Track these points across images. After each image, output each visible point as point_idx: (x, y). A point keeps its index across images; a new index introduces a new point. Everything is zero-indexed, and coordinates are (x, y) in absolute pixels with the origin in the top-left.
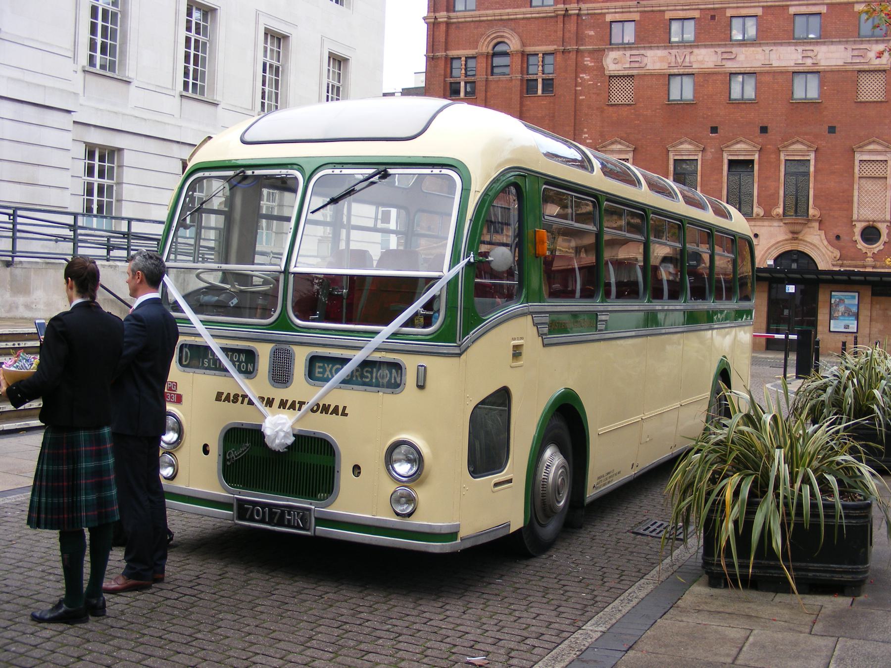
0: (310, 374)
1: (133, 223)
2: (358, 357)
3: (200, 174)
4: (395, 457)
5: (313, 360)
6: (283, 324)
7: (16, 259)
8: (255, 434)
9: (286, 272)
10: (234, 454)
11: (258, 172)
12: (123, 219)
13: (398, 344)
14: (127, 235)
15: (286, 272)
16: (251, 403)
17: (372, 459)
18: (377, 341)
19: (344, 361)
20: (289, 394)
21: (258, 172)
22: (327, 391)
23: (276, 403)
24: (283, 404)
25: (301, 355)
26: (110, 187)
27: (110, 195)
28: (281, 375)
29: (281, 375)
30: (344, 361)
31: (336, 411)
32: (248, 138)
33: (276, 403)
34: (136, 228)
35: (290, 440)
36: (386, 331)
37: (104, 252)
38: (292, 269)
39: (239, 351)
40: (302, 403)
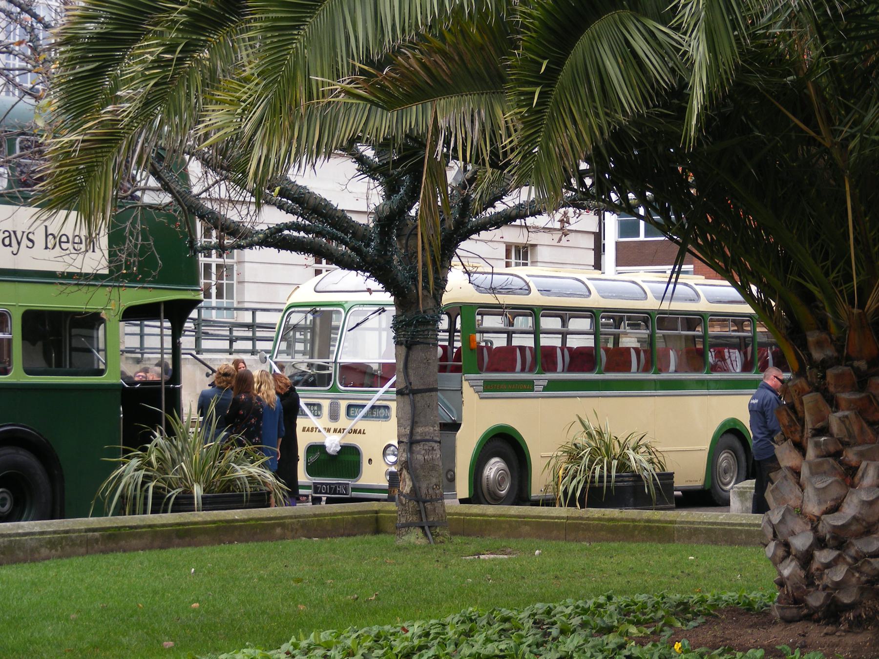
0: (348, 414)
1: (258, 313)
2: (370, 404)
3: (292, 309)
4: (388, 452)
5: (349, 407)
6: (334, 389)
7: (146, 356)
8: (321, 448)
9: (335, 362)
10: (312, 459)
11: (322, 309)
12: (247, 309)
13: (388, 396)
14: (251, 326)
15: (335, 362)
16: (320, 431)
17: (377, 455)
18: (377, 396)
19: (363, 406)
20: (338, 425)
21: (322, 309)
22: (358, 423)
23: (332, 430)
24: (335, 431)
25: (343, 404)
26: (230, 268)
27: (230, 276)
28: (334, 416)
29: (334, 416)
30: (363, 406)
31: (360, 432)
32: (318, 289)
33: (332, 430)
34: (261, 318)
35: (339, 448)
36: (382, 390)
37: (225, 345)
38: (339, 360)
39: (314, 405)
40: (344, 429)
